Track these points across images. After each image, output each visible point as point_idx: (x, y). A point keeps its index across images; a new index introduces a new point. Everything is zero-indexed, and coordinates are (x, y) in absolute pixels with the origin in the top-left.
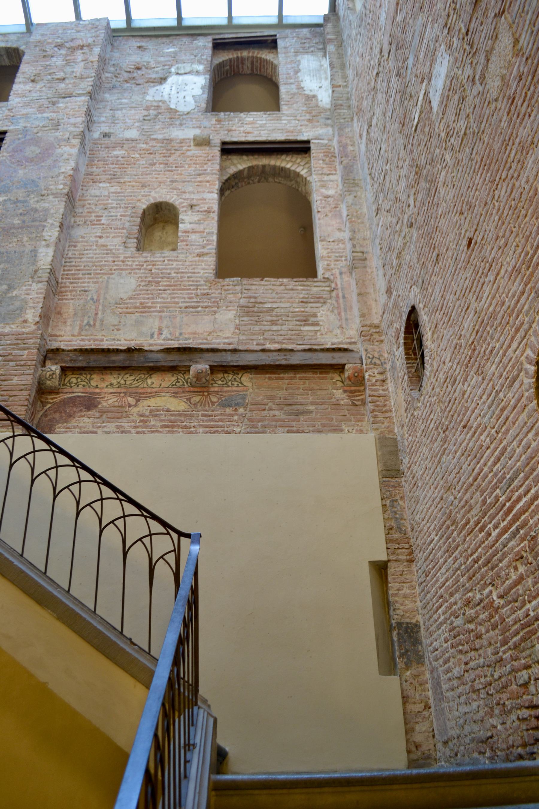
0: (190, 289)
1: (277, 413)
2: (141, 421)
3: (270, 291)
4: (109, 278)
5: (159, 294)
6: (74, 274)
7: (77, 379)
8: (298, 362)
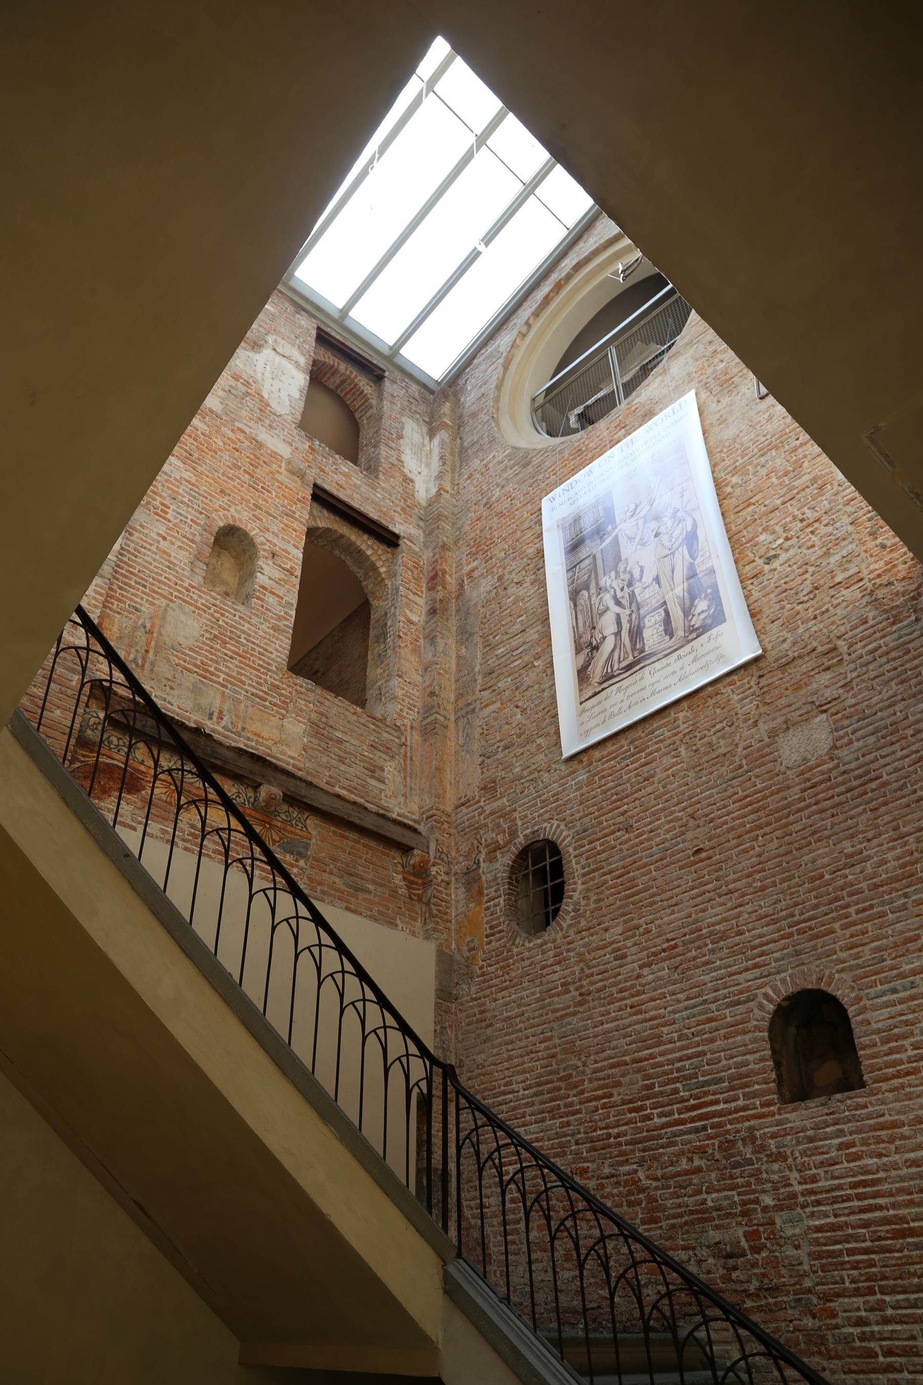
0: (259, 671)
1: (337, 880)
3: (343, 717)
4: (168, 605)
5: (224, 659)
7: (119, 739)
8: (370, 827)
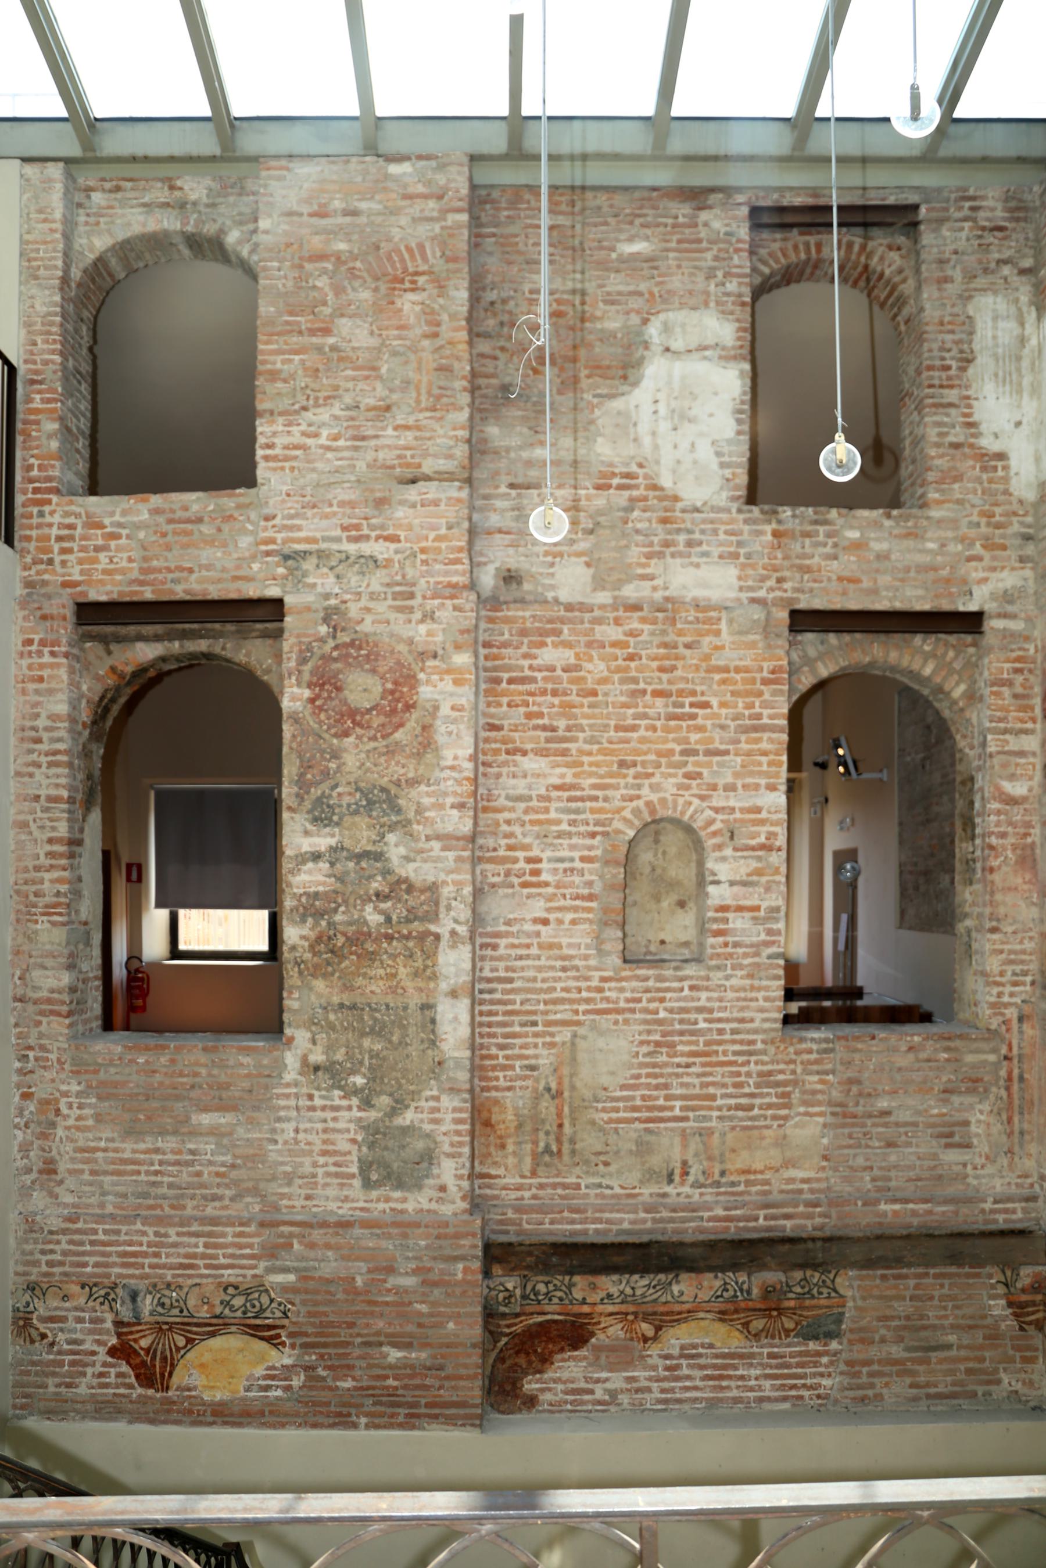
2: (667, 1368)
4: (575, 1035)
6: (504, 1024)
7: (547, 1284)
